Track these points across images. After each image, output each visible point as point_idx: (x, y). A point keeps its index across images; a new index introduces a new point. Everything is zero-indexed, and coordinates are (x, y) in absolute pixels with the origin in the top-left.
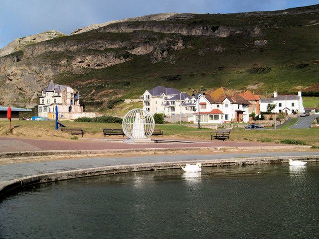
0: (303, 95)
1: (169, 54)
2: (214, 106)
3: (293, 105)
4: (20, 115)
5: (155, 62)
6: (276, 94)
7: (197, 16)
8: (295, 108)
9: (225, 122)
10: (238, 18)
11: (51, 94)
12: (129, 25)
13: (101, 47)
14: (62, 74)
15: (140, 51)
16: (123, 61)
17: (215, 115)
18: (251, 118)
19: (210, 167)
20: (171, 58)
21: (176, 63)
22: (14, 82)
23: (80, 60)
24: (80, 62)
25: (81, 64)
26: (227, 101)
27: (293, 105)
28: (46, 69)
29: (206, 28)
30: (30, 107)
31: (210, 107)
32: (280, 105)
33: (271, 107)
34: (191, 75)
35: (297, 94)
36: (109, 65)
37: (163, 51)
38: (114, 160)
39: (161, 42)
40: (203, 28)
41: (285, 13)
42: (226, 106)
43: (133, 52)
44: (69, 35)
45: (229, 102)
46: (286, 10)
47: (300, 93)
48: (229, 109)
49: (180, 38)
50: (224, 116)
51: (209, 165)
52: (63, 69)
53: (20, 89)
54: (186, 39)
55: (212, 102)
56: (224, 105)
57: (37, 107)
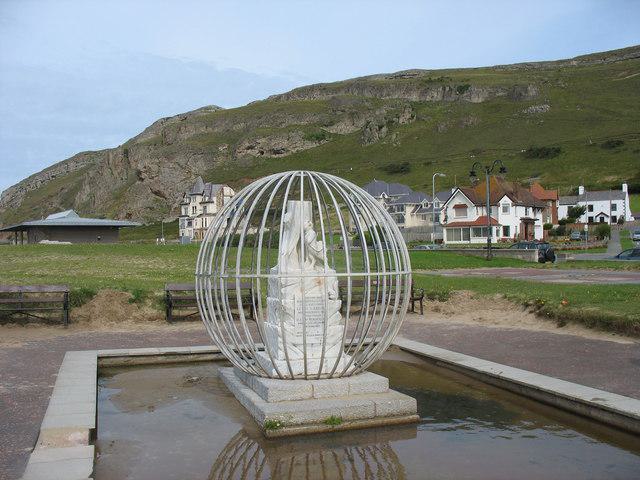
0: (631, 191)
1: (390, 132)
2: (482, 212)
3: (614, 207)
4: (120, 230)
5: (368, 144)
6: (581, 190)
7: (432, 72)
8: (618, 214)
9: (504, 241)
10: (498, 73)
11: (199, 199)
12: (612, 145)
13: (281, 124)
14: (220, 168)
15: (344, 128)
16: (310, 145)
17: (484, 227)
18: (547, 231)
19: (212, 361)
20: (394, 137)
21: (402, 144)
22: (147, 181)
23: (247, 145)
24: (248, 148)
25: (249, 151)
26: (506, 200)
27: (614, 207)
28: (196, 161)
29: (447, 89)
30: (169, 220)
31: (474, 214)
32: (591, 208)
33: (575, 213)
34: (428, 164)
35: (621, 189)
36: (294, 151)
37: (380, 128)
38: (19, 345)
39: (377, 113)
40: (444, 89)
41: (575, 63)
42: (505, 210)
43: (332, 130)
44: (227, 107)
45: (510, 202)
46: (575, 59)
47: (625, 187)
48: (510, 217)
49: (408, 105)
50: (501, 229)
51: (210, 357)
52: (220, 161)
53: (156, 193)
54: (415, 106)
55: (479, 204)
56: (500, 209)
57: (177, 220)
